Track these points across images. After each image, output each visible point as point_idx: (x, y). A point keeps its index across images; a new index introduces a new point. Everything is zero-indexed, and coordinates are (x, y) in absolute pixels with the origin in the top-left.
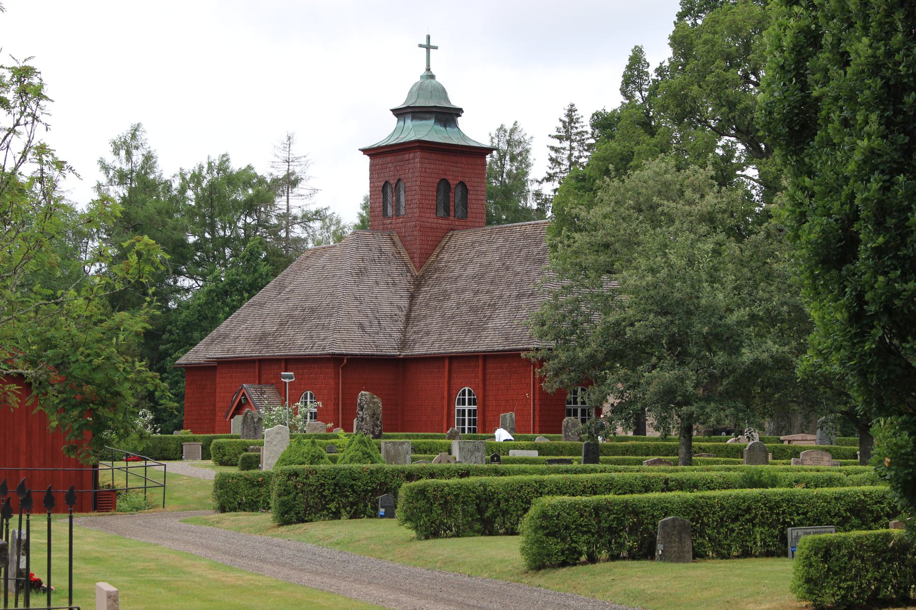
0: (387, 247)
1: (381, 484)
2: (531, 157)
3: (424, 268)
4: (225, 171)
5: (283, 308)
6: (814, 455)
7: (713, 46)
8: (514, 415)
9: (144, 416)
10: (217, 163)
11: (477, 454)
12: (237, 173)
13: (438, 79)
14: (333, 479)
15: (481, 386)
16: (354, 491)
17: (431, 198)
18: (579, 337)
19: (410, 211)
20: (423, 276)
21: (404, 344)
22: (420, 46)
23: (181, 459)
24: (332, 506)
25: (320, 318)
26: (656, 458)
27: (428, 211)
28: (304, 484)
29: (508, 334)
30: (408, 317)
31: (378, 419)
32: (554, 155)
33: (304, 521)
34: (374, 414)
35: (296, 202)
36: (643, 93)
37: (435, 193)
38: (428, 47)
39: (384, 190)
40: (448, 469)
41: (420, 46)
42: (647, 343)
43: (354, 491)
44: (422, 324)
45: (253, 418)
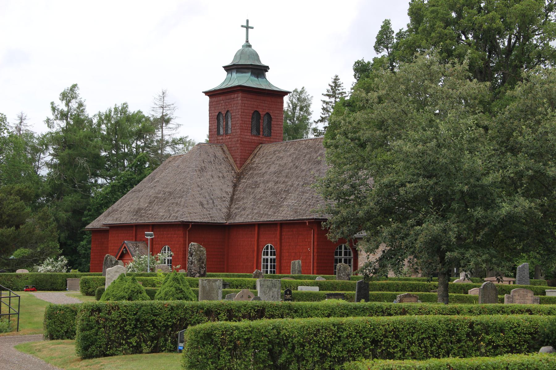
0: (220, 154)
1: (181, 320)
2: (311, 109)
3: (243, 168)
4: (125, 113)
5: (152, 192)
6: (521, 292)
7: (437, 14)
8: (300, 262)
9: (62, 261)
10: (120, 108)
11: (274, 289)
12: (132, 115)
13: (253, 47)
14: (135, 314)
15: (279, 243)
16: (155, 326)
17: (248, 123)
18: (357, 197)
19: (234, 131)
20: (242, 173)
21: (229, 216)
22: (242, 26)
23: (65, 290)
24: (133, 341)
25: (175, 198)
26: (406, 293)
27: (246, 131)
28: (106, 319)
29: (296, 209)
30: (232, 199)
31: (203, 263)
32: (325, 106)
33: (105, 355)
34: (200, 259)
35: (168, 133)
36: (389, 50)
37: (251, 120)
38: (247, 27)
39: (218, 119)
40: (245, 306)
41: (242, 26)
42: (412, 201)
43: (155, 326)
44: (241, 203)
45: (111, 261)
